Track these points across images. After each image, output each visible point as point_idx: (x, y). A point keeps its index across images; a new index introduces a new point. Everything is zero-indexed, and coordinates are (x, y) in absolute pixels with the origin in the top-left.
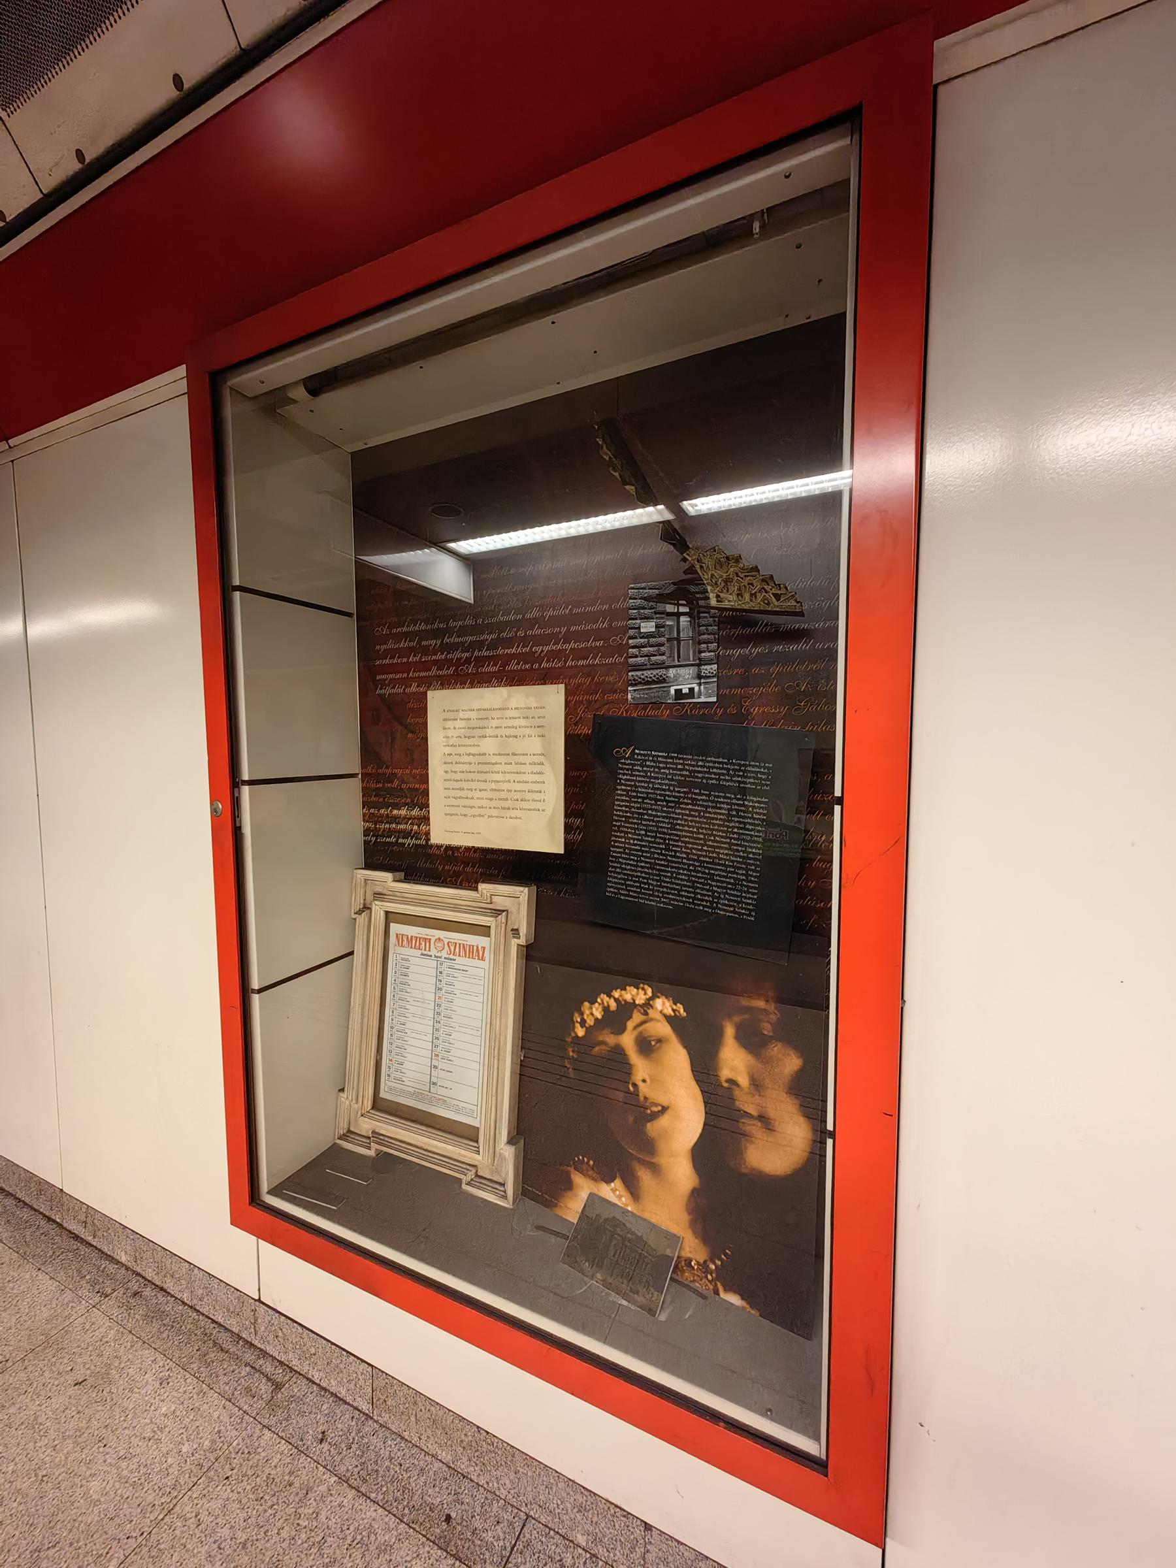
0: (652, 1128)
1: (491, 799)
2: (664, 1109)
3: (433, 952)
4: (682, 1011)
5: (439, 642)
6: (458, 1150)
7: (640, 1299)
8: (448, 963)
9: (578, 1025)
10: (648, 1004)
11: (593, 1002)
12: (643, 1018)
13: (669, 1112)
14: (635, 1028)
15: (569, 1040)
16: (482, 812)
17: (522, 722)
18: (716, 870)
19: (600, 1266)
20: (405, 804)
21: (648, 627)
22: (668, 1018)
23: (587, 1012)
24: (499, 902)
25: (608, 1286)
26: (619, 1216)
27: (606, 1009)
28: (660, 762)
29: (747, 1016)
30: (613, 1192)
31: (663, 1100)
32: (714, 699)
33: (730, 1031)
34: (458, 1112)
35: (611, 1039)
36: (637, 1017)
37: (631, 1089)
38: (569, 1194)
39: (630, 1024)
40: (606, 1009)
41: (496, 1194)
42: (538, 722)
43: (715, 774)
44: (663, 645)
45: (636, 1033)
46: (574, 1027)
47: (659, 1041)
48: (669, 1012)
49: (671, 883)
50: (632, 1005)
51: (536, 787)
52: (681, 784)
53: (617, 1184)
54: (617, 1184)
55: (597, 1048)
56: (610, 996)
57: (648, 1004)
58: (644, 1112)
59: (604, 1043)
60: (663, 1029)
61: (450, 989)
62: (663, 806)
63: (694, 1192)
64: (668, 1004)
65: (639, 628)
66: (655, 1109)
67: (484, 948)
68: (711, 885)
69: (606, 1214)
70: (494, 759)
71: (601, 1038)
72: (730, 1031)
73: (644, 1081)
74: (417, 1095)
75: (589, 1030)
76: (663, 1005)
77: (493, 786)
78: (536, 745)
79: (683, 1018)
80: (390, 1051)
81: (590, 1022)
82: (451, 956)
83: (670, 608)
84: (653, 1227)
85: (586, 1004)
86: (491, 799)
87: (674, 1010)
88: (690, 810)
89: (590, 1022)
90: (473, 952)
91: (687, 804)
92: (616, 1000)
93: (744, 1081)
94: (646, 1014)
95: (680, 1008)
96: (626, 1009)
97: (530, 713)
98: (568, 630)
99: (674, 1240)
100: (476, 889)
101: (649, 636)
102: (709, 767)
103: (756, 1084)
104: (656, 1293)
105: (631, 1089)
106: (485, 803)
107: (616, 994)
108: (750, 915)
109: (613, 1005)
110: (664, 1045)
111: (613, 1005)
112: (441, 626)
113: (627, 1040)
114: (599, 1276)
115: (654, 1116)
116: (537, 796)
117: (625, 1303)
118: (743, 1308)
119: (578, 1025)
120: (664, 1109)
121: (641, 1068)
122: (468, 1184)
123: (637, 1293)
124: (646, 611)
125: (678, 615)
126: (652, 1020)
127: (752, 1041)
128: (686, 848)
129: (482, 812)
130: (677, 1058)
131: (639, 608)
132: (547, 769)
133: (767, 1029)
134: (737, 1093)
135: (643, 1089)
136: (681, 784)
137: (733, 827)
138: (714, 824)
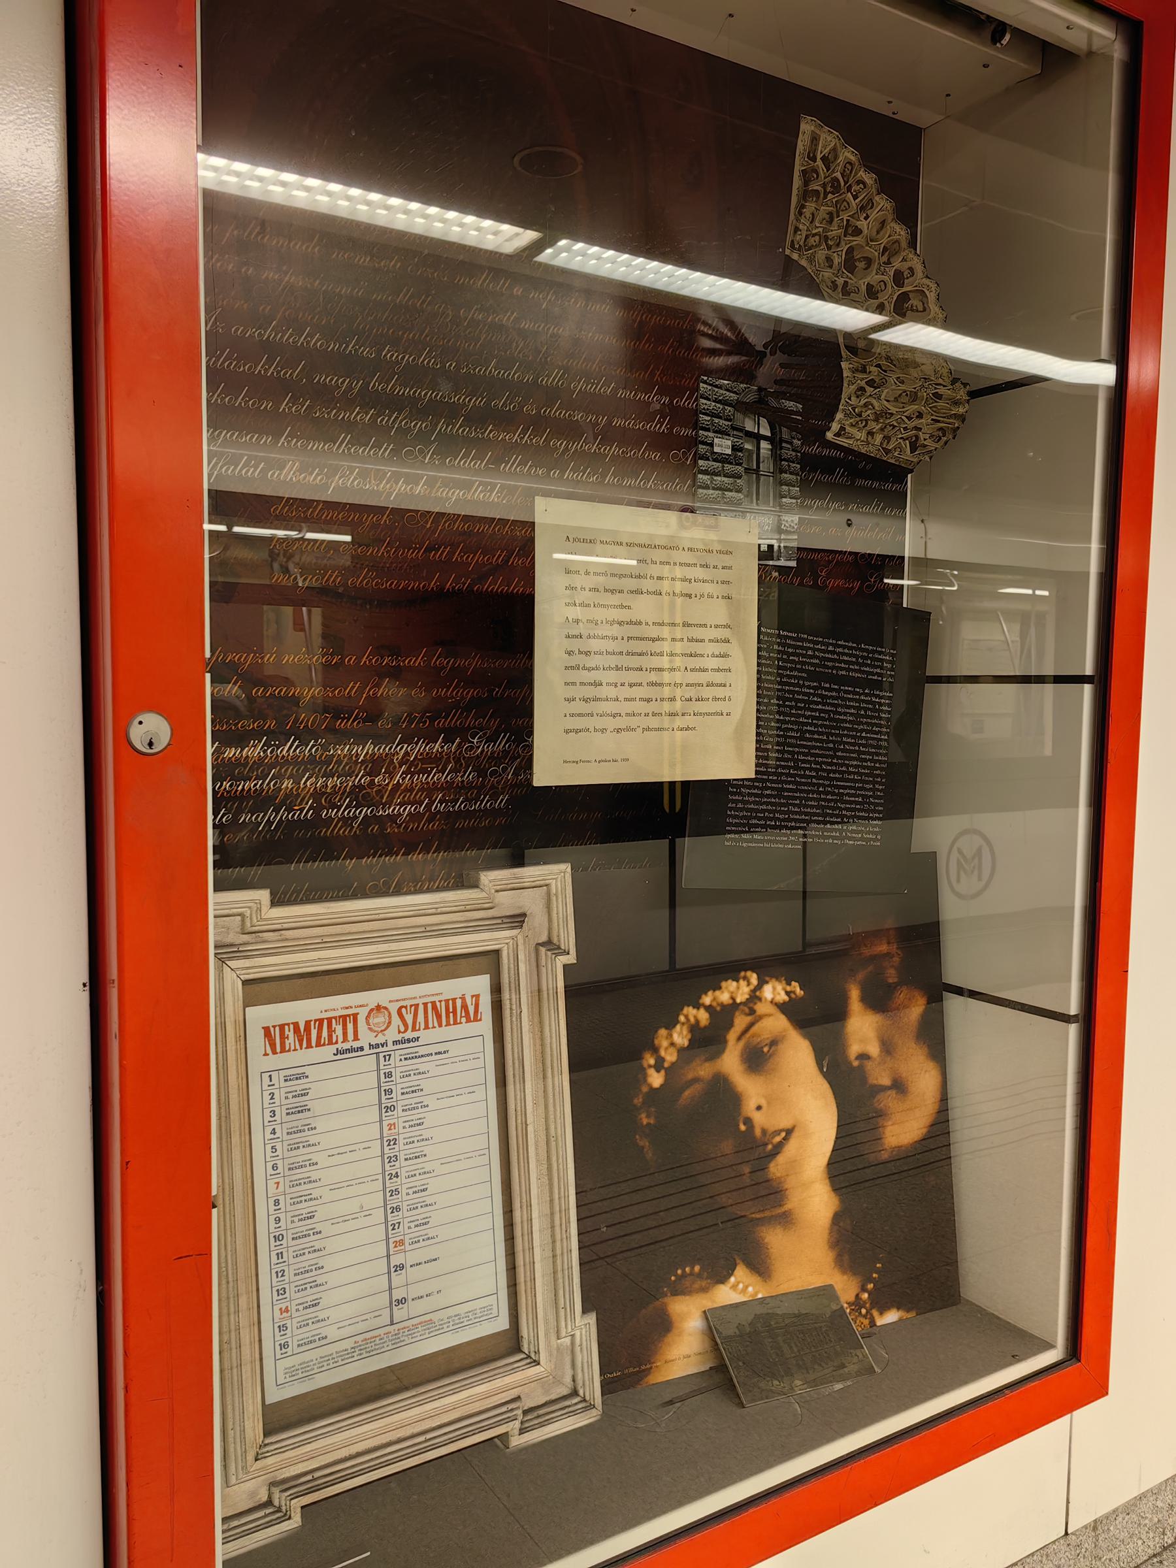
0: (776, 1168)
1: (648, 700)
2: (789, 1132)
3: (366, 1038)
4: (798, 989)
5: (358, 386)
6: (498, 1383)
7: (852, 1368)
8: (408, 1049)
9: (652, 1072)
10: (755, 997)
11: (671, 1025)
12: (749, 1019)
13: (795, 1135)
14: (739, 1039)
15: (638, 1101)
16: (633, 722)
17: (699, 573)
18: (845, 788)
19: (789, 1373)
20: (257, 735)
21: (723, 446)
22: (783, 1008)
23: (665, 1043)
24: (507, 903)
25: (814, 1383)
26: (760, 1310)
27: (694, 1028)
28: (790, 646)
29: (870, 968)
30: (737, 1290)
31: (785, 1123)
32: (793, 564)
33: (855, 994)
34: (459, 1328)
35: (704, 1070)
36: (741, 1021)
37: (743, 1128)
38: (670, 1338)
39: (732, 1036)
40: (694, 1028)
41: (574, 1413)
42: (723, 575)
43: (846, 662)
44: (740, 477)
45: (742, 1043)
46: (645, 1076)
47: (774, 1043)
48: (782, 997)
49: (800, 813)
50: (734, 1006)
51: (718, 678)
52: (812, 676)
53: (741, 1273)
54: (741, 1273)
55: (687, 1093)
56: (697, 1006)
57: (755, 997)
58: (760, 1151)
59: (696, 1080)
60: (777, 1023)
61: (412, 1100)
62: (791, 707)
63: (837, 1218)
64: (780, 987)
65: (711, 445)
66: (778, 1139)
67: (477, 996)
68: (841, 809)
69: (745, 1318)
70: (653, 632)
71: (690, 1076)
72: (855, 994)
73: (759, 1108)
74: (365, 1348)
75: (671, 1072)
76: (774, 991)
77: (653, 677)
78: (718, 612)
79: (802, 998)
80: (282, 1292)
81: (670, 1057)
82: (409, 1035)
83: (749, 426)
84: (800, 1294)
85: (663, 1032)
86: (648, 700)
87: (787, 993)
88: (821, 711)
89: (670, 1057)
90: (451, 1012)
91: (817, 703)
92: (708, 1008)
93: (874, 1050)
94: (752, 1012)
95: (796, 987)
96: (723, 1016)
97: (712, 560)
98: (610, 422)
99: (827, 1292)
100: (475, 885)
101: (722, 459)
102: (839, 654)
103: (888, 1048)
104: (858, 1352)
105: (743, 1128)
106: (639, 707)
107: (707, 1000)
108: (876, 840)
109: (703, 1016)
110: (780, 1046)
111: (703, 1016)
112: (365, 352)
113: (731, 1062)
114: (798, 1382)
115: (778, 1148)
116: (720, 692)
117: (838, 1386)
118: (900, 1320)
119: (652, 1072)
120: (789, 1132)
121: (752, 1091)
122: (522, 1431)
123: (843, 1366)
124: (722, 422)
125: (758, 437)
126: (761, 1018)
127: (879, 1000)
128: (817, 763)
129: (633, 722)
130: (798, 1053)
131: (713, 415)
132: (734, 649)
133: (892, 976)
134: (869, 1065)
135: (758, 1119)
136: (812, 676)
137: (862, 731)
138: (844, 729)
